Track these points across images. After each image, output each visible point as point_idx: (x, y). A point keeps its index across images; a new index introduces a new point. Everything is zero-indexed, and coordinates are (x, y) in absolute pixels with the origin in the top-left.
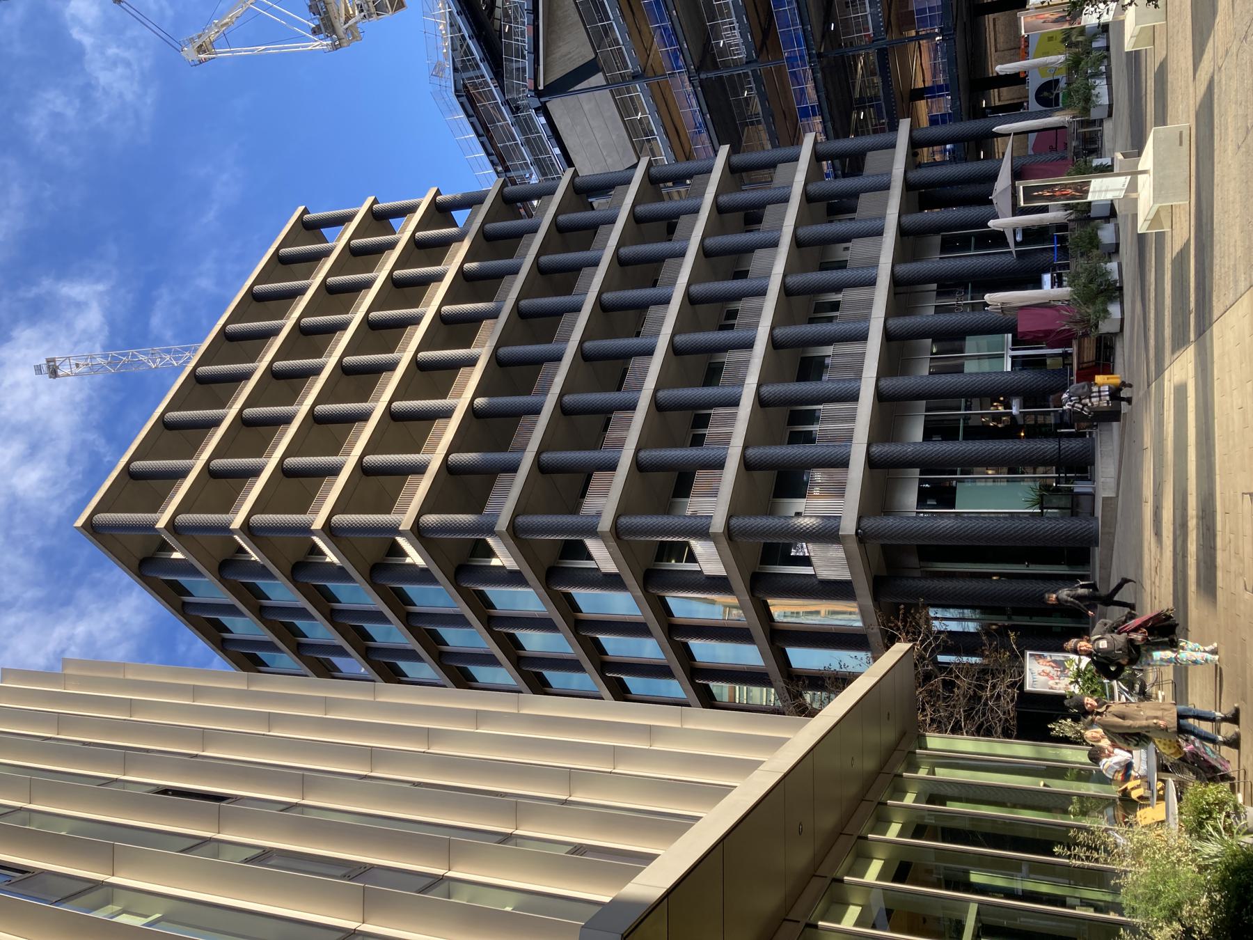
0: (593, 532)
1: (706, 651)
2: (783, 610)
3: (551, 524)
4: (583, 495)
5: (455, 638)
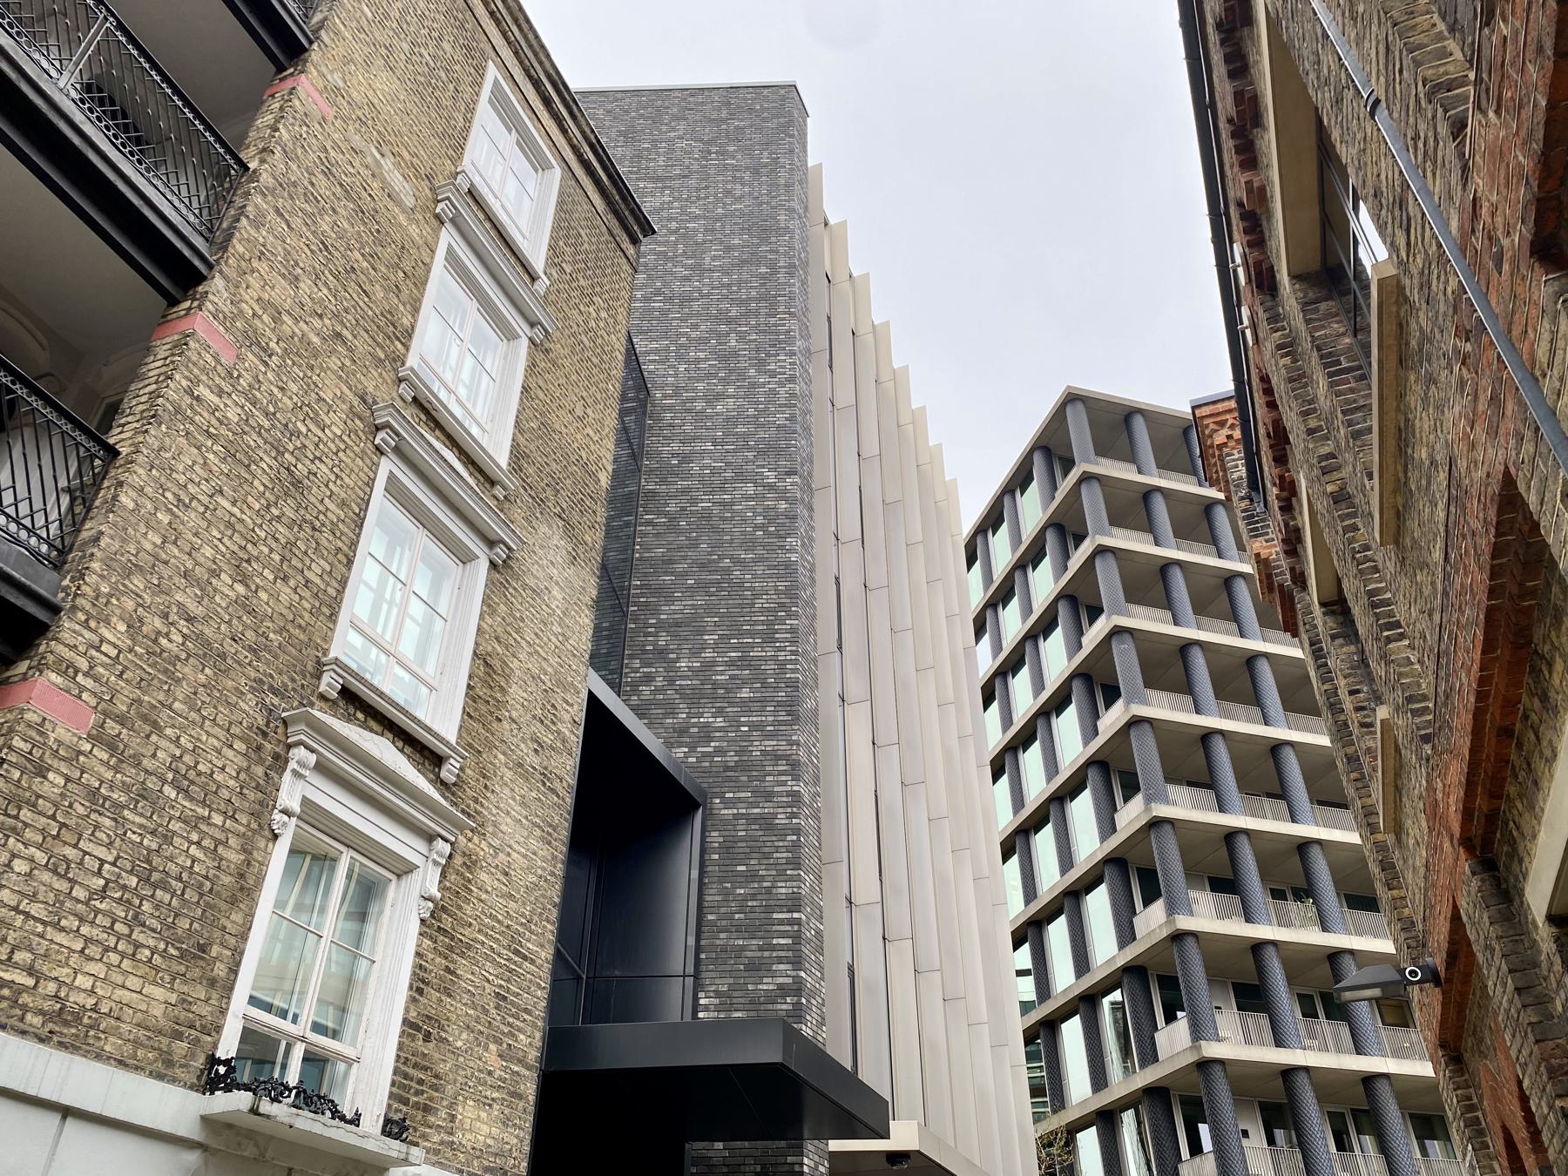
0: (1171, 909)
1: (1058, 933)
2: (1098, 904)
3: (1146, 756)
4: (1190, 784)
5: (1021, 684)
